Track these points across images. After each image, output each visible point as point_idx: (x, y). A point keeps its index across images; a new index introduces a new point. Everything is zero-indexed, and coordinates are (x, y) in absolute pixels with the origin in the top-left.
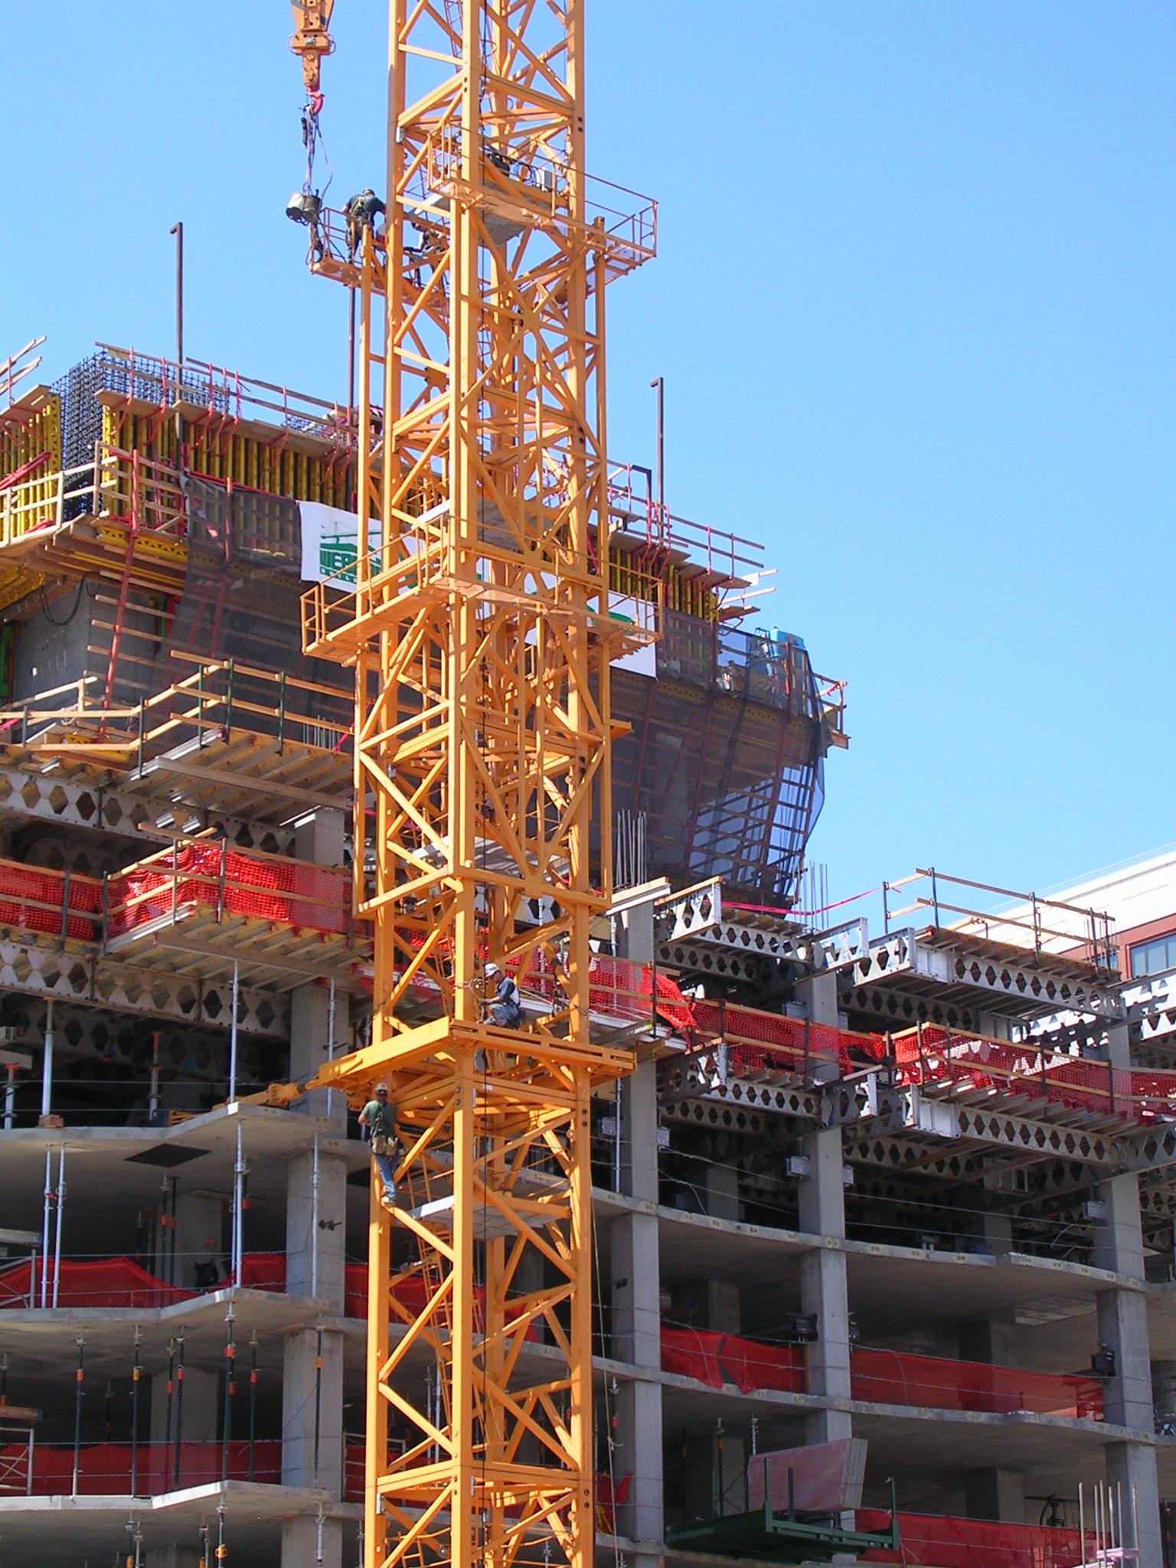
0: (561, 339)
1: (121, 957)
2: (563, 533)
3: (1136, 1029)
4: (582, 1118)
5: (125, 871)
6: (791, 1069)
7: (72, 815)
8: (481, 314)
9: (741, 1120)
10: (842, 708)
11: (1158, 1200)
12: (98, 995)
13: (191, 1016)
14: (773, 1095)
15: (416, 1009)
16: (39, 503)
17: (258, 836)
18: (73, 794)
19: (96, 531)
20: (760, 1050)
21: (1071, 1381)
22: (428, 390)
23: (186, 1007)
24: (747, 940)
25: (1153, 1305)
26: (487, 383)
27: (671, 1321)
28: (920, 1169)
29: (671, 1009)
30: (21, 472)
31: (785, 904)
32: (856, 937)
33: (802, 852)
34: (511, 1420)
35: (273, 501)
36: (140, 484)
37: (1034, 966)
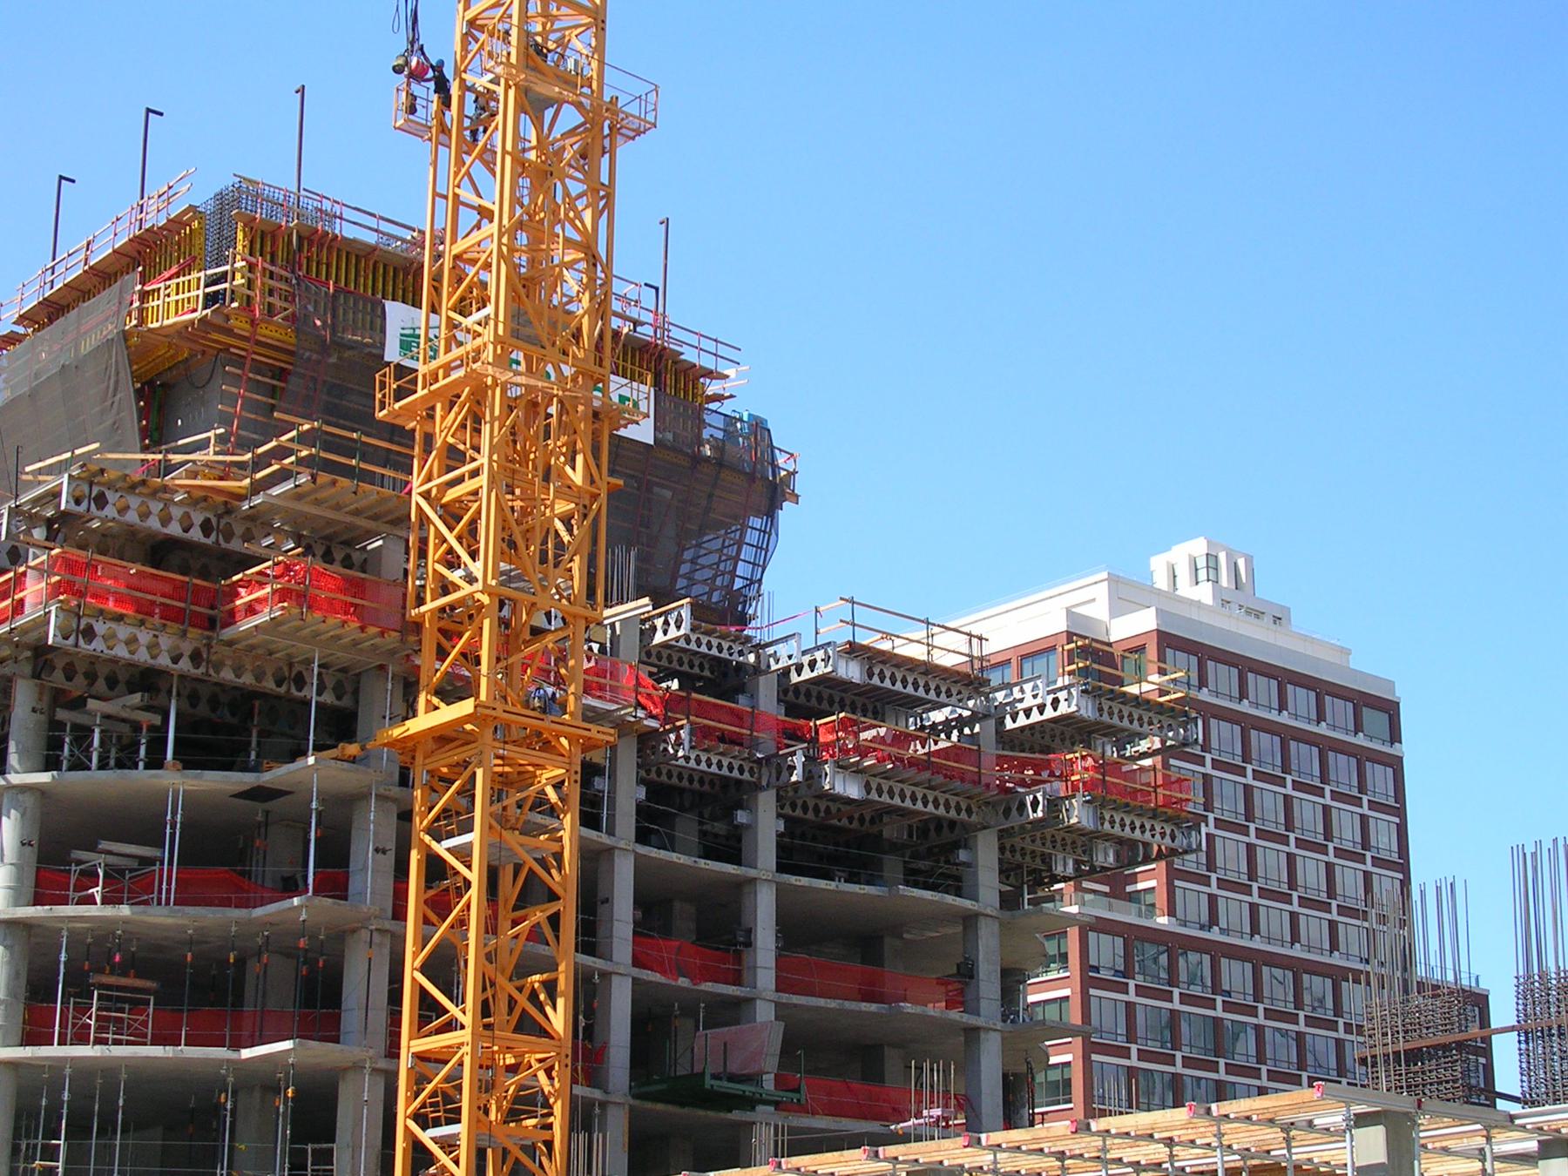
0: (581, 188)
1: (230, 643)
2: (577, 335)
3: (1001, 722)
4: (574, 777)
5: (235, 578)
6: (741, 745)
7: (196, 535)
8: (521, 166)
9: (701, 781)
10: (794, 473)
11: (1013, 850)
12: (211, 672)
13: (282, 690)
14: (725, 764)
15: (451, 691)
16: (187, 295)
17: (338, 555)
18: (198, 518)
19: (228, 318)
20: (715, 729)
21: (942, 982)
22: (479, 222)
23: (279, 684)
24: (710, 646)
25: (1006, 929)
26: (525, 217)
27: (642, 930)
28: (835, 822)
29: (649, 696)
30: (175, 269)
31: (743, 620)
32: (791, 647)
33: (760, 581)
34: (512, 1003)
35: (366, 300)
36: (263, 284)
37: (925, 673)
